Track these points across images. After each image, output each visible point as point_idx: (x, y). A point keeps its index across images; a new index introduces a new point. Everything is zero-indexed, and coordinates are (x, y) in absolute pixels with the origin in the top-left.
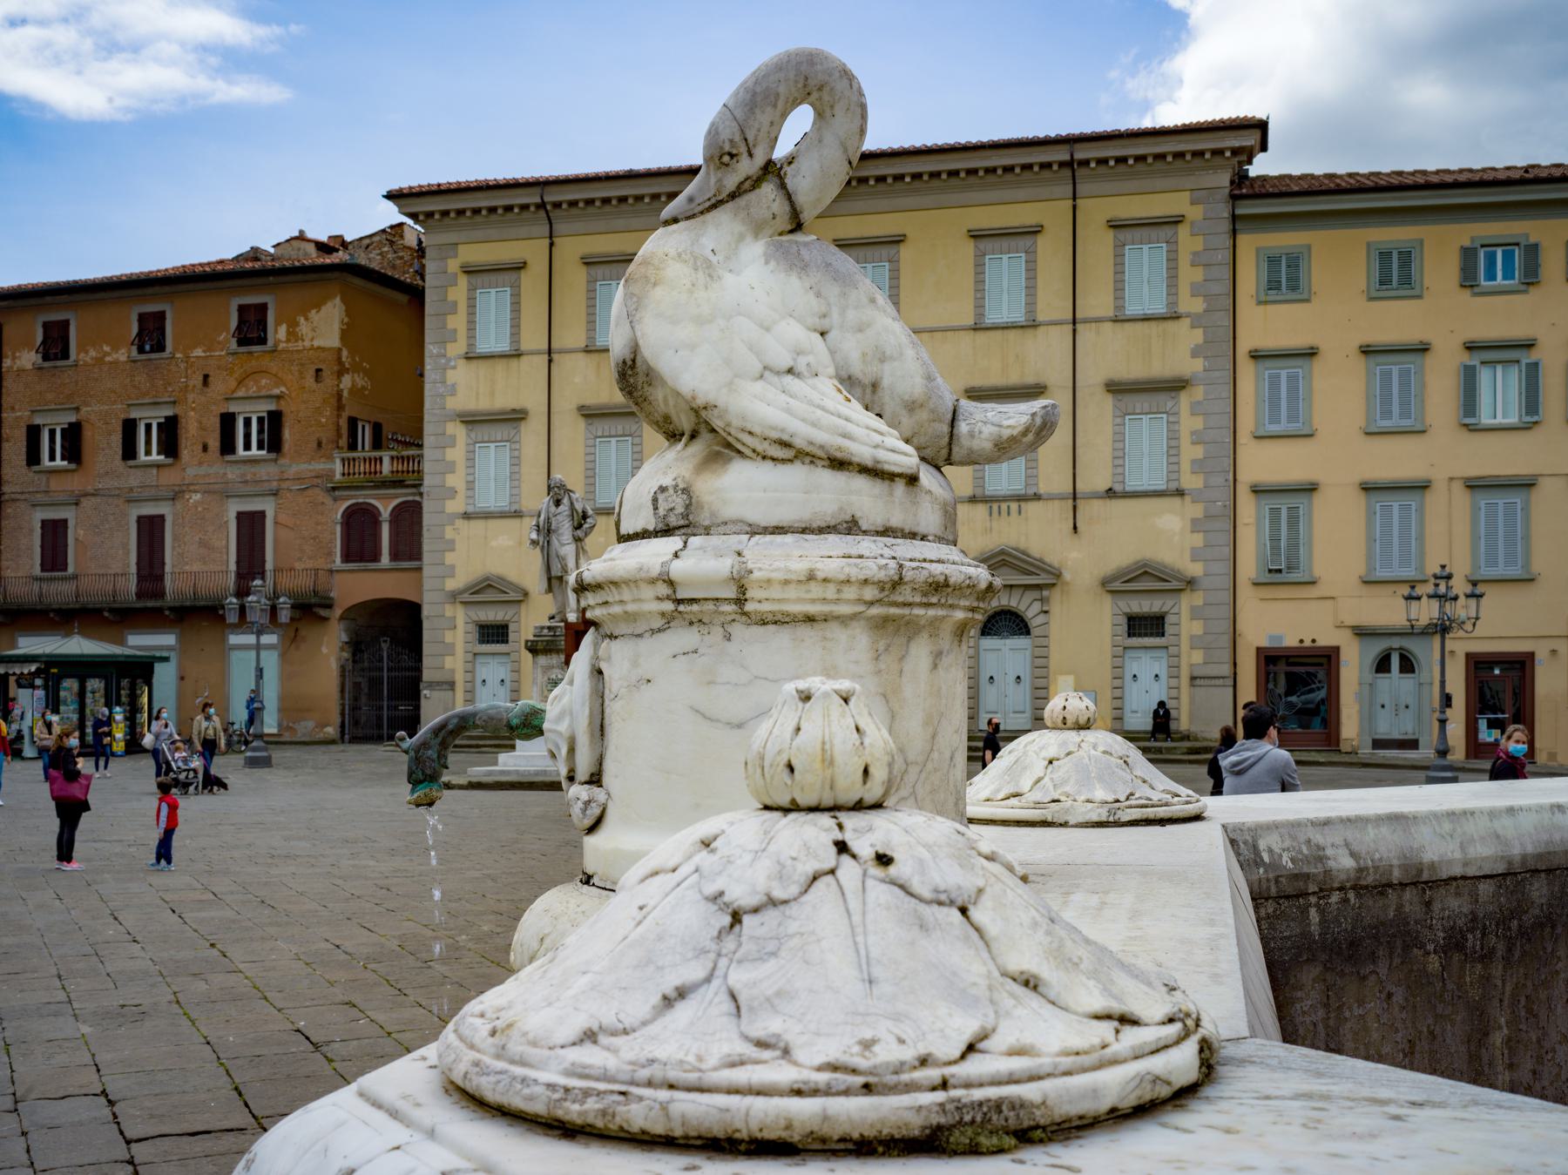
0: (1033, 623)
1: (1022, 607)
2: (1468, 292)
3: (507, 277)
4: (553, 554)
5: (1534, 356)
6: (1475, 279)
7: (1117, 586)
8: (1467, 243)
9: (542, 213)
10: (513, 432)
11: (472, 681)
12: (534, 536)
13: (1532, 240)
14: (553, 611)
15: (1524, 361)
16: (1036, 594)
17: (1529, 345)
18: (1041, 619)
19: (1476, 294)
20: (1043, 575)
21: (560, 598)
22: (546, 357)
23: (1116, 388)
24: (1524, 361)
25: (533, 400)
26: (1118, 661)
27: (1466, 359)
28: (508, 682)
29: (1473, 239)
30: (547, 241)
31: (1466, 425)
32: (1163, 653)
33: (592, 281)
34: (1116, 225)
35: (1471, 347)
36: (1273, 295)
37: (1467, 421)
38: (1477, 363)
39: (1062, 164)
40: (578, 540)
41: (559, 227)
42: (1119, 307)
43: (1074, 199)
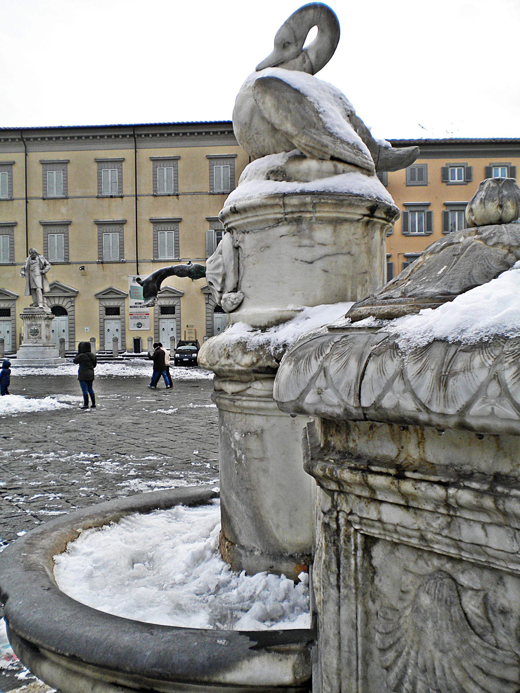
0: (68, 310)
1: (64, 305)
2: (445, 184)
3: (171, 163)
4: (31, 279)
5: (430, 209)
6: (448, 179)
7: (101, 296)
8: (444, 166)
9: (22, 143)
10: (10, 231)
11: (104, 330)
12: (23, 273)
13: (469, 166)
14: (32, 303)
15: (426, 211)
16: (69, 300)
17: (428, 205)
18: (71, 309)
19: (447, 185)
20: (71, 292)
21: (34, 297)
22: (25, 201)
23: (45, 225)
24: (426, 211)
25: (20, 219)
26: (156, 324)
27: (444, 209)
28: (10, 332)
29: (446, 164)
30: (24, 154)
31: (404, 234)
32: (174, 320)
33: (45, 171)
34: (43, 163)
35: (446, 205)
36: (413, 183)
37: (404, 233)
38: (408, 211)
39: (19, 139)
40: (43, 274)
41: (29, 148)
42: (155, 189)
43: (136, 149)
